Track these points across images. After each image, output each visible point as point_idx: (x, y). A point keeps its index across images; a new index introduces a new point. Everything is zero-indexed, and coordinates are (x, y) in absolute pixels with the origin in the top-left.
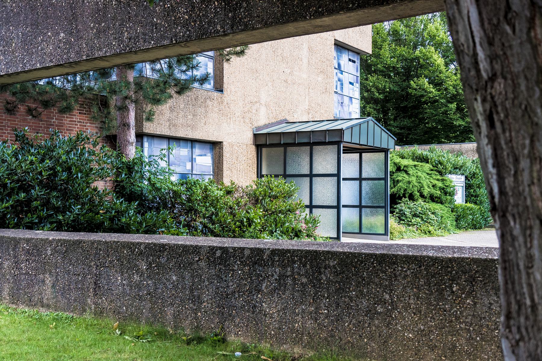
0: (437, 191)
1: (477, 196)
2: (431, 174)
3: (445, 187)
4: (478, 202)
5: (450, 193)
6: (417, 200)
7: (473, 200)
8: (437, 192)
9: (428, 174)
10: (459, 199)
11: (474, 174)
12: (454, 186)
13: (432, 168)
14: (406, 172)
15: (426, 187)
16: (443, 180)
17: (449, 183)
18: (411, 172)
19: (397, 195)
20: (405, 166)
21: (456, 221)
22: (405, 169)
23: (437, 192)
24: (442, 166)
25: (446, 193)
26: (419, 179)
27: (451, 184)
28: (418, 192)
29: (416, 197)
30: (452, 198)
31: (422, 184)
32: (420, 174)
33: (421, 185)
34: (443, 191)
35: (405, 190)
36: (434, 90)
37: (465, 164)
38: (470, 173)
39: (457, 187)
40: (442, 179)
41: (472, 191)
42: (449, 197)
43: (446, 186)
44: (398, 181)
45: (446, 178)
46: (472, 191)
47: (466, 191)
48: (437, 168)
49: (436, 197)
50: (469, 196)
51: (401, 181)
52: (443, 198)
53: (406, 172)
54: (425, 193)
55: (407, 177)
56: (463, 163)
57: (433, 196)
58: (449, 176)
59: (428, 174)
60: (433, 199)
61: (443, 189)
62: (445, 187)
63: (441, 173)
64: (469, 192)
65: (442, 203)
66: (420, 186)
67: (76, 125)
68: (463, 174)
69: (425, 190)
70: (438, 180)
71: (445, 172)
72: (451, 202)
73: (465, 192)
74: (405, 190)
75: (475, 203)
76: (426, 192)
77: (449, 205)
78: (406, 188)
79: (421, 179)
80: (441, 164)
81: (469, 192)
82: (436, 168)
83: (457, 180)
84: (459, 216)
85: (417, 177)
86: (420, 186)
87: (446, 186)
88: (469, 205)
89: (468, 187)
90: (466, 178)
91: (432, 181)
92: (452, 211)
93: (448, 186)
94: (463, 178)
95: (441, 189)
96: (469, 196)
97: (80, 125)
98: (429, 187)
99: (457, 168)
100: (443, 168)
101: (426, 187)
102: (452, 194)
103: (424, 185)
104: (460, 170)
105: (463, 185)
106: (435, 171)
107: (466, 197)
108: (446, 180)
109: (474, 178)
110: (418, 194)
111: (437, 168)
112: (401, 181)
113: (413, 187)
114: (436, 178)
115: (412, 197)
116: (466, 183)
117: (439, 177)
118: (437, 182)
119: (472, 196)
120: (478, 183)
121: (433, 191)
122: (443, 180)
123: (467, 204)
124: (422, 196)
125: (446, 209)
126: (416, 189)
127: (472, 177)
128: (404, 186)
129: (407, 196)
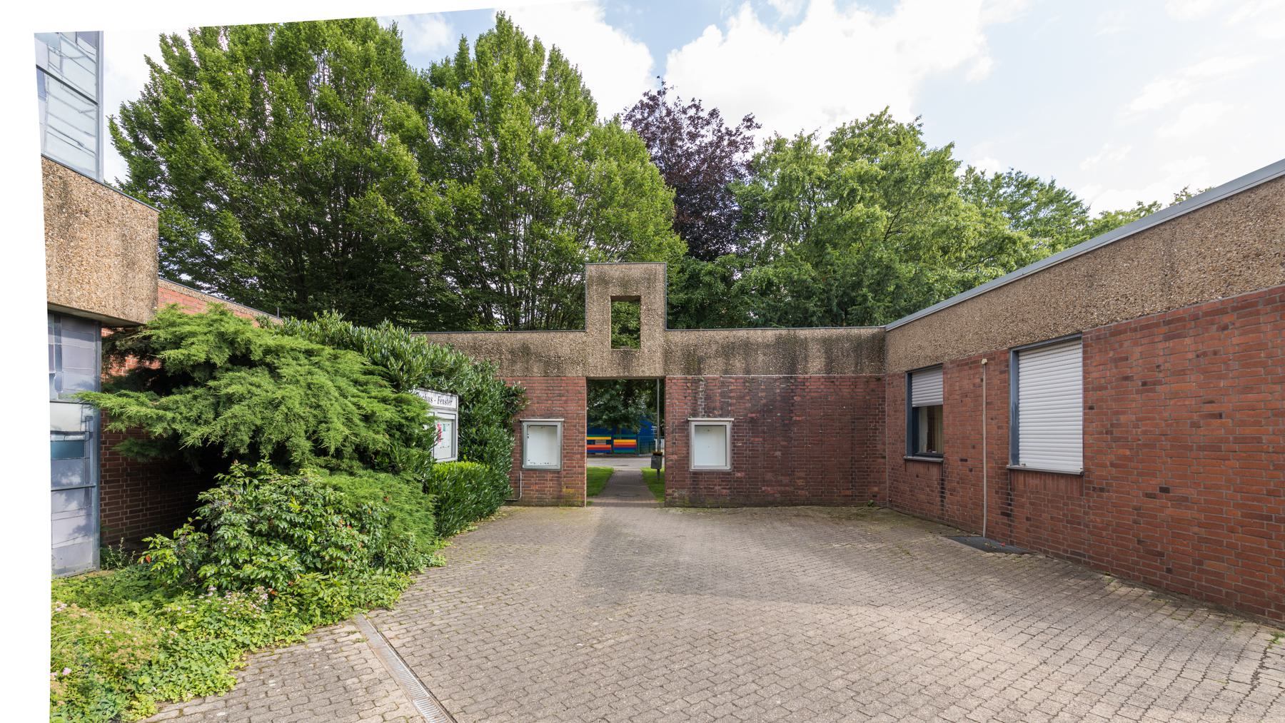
0: (378, 433)
1: (483, 443)
2: (366, 383)
3: (403, 421)
4: (485, 455)
5: (419, 440)
6: (299, 465)
7: (476, 450)
8: (380, 437)
9: (356, 382)
10: (444, 451)
11: (478, 393)
12: (432, 419)
13: (372, 367)
14: (273, 371)
15: (338, 424)
16: (399, 402)
17: (417, 410)
18: (284, 371)
19: (226, 450)
20: (268, 351)
21: (437, 514)
22: (269, 359)
23: (380, 437)
24: (401, 364)
25: (407, 441)
26: (314, 396)
27: (422, 412)
28: (308, 438)
29: (296, 457)
30: (426, 453)
31: (324, 411)
32: (321, 378)
33: (320, 415)
34: (398, 434)
35: (258, 431)
36: (396, 219)
37: (460, 366)
38: (469, 391)
39: (441, 423)
40: (395, 399)
41: (474, 430)
42: (415, 451)
43: (406, 418)
44: (230, 400)
45: (410, 397)
46: (474, 430)
47: (460, 430)
48: (386, 366)
49: (377, 453)
50: (466, 442)
51: (241, 398)
52: (399, 452)
53: (273, 371)
54: (332, 443)
55: (270, 387)
56: (455, 362)
57: (366, 449)
58: (422, 394)
59: (356, 382)
60: (367, 457)
61: (400, 427)
62: (403, 421)
63: (396, 384)
64: (466, 433)
65: (393, 469)
66: (315, 416)
67: (1066, 551)
68: (454, 392)
69: (332, 433)
70: (384, 400)
71: (408, 381)
72: (424, 463)
73: (459, 434)
74: (258, 431)
75: (481, 458)
76: (336, 434)
77: (416, 476)
78: (259, 422)
79: (322, 394)
80: (397, 356)
81: (466, 433)
82: (381, 368)
83: (441, 405)
84: (443, 501)
85: (309, 386)
86: (315, 416)
87: (406, 418)
88: (468, 465)
89: (465, 421)
90: (462, 401)
91: (363, 403)
92: (426, 490)
93: (412, 420)
94: (454, 403)
95: (392, 428)
96: (466, 442)
97: (1144, 565)
98: (349, 421)
99: (440, 374)
100: (401, 369)
101: (338, 424)
102: (426, 442)
103: (332, 415)
104: (447, 378)
105: (453, 417)
106: (379, 375)
107: (460, 444)
108: (408, 402)
109: (478, 402)
110: (307, 445)
111: (386, 366)
112: (241, 398)
113: (287, 419)
114: (379, 395)
115: (283, 459)
116: (460, 413)
117: (388, 392)
118: (378, 407)
119: (474, 441)
120: (486, 413)
121: (365, 433)
122: (399, 402)
123: (462, 463)
124: (319, 450)
125: (406, 489)
126: (300, 427)
127: (473, 400)
128: (249, 417)
129: (266, 450)
